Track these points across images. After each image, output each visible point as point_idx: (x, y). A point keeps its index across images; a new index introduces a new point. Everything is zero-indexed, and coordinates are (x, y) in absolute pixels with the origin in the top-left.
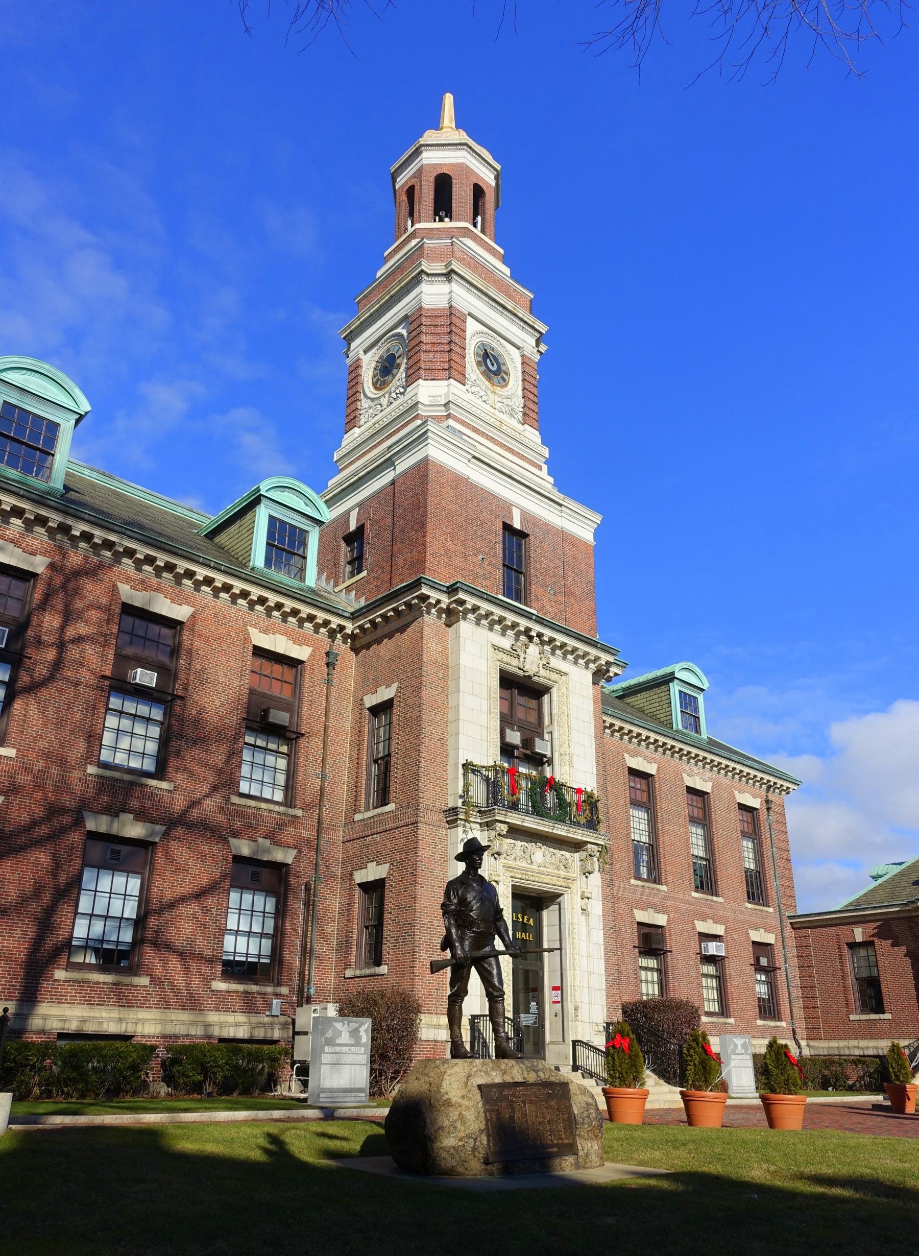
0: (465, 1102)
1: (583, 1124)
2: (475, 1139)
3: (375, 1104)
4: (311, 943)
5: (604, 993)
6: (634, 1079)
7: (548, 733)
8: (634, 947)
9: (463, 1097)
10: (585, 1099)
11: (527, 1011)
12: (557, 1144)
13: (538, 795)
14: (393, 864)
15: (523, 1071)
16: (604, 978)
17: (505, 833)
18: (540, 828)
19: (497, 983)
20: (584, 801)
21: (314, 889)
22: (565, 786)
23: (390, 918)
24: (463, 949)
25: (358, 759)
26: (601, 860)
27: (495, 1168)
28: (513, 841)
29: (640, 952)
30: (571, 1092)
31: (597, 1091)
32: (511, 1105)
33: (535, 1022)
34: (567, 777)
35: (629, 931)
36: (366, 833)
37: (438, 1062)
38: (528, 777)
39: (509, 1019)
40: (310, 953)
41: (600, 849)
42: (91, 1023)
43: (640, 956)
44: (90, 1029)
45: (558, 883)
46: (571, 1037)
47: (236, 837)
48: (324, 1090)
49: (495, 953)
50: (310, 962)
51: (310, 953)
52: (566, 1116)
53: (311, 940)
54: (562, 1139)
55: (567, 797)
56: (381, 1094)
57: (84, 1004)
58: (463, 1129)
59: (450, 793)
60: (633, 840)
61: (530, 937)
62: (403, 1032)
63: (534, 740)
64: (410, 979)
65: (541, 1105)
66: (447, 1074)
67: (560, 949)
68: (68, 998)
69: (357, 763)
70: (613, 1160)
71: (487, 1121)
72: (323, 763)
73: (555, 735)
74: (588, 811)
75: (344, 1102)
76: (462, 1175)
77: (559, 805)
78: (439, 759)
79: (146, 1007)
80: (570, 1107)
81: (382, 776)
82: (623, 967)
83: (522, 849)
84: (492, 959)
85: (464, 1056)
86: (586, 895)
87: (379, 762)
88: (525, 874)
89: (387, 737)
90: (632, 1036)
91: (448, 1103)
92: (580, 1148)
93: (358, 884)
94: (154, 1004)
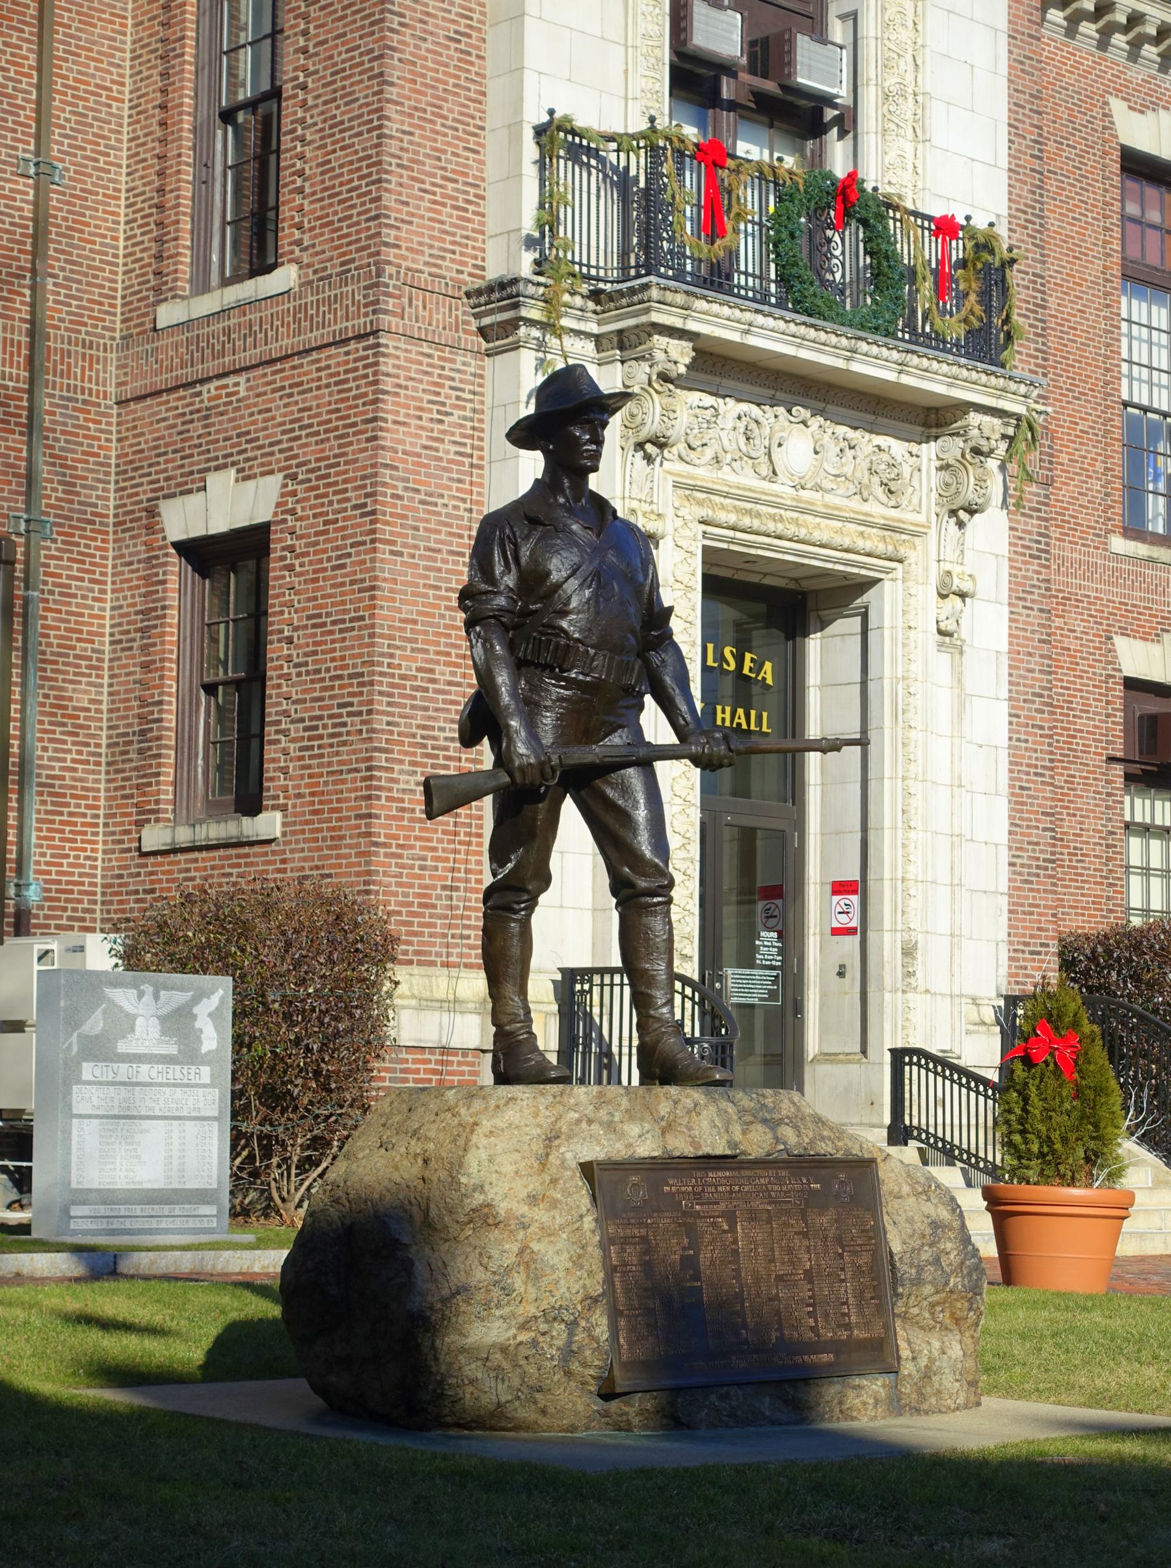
0: (540, 1215)
1: (918, 1282)
2: (572, 1325)
3: (249, 1238)
4: (22, 738)
5: (1003, 902)
6: (1087, 1159)
7: (842, 17)
8: (1111, 759)
9: (533, 1200)
10: (928, 1208)
11: (747, 959)
12: (831, 1340)
13: (803, 241)
14: (294, 477)
15: (728, 1123)
16: (1004, 856)
17: (682, 369)
18: (804, 354)
19: (647, 851)
20: (963, 264)
21: (27, 563)
22: (896, 208)
23: (289, 659)
24: (533, 736)
25: (163, 107)
26: (1012, 467)
27: (633, 1409)
28: (709, 400)
29: (1129, 778)
30: (884, 1189)
31: (973, 1201)
32: (688, 1225)
33: (772, 995)
34: (906, 177)
35: (1096, 706)
36: (200, 370)
37: (450, 1094)
38: (766, 176)
39: (686, 981)
40: (21, 773)
41: (1010, 431)
43: (1124, 289)
45: (861, 544)
46: (888, 1038)
48: (83, 1197)
49: (642, 752)
50: (20, 801)
51: (21, 773)
52: (864, 1259)
53: (23, 729)
54: (848, 1327)
55: (904, 250)
56: (269, 1210)
58: (532, 1293)
59: (490, 229)
60: (1126, 404)
61: (761, 721)
62: (336, 1019)
63: (792, 42)
64: (358, 854)
65: (786, 1224)
66: (479, 1130)
67: (863, 742)
69: (163, 124)
70: (1008, 1391)
71: (610, 1271)
72: (38, 121)
73: (870, 26)
74: (973, 297)
75: (150, 1232)
76: (528, 1428)
77: (876, 276)
78: (451, 109)
80: (876, 1234)
81: (251, 171)
82: (1068, 826)
83: (741, 426)
84: (631, 771)
85: (539, 1076)
86: (957, 584)
87: (241, 117)
88: (749, 512)
89: (267, 29)
90: (1087, 1027)
91: (485, 1217)
92: (905, 1353)
93: (175, 545)
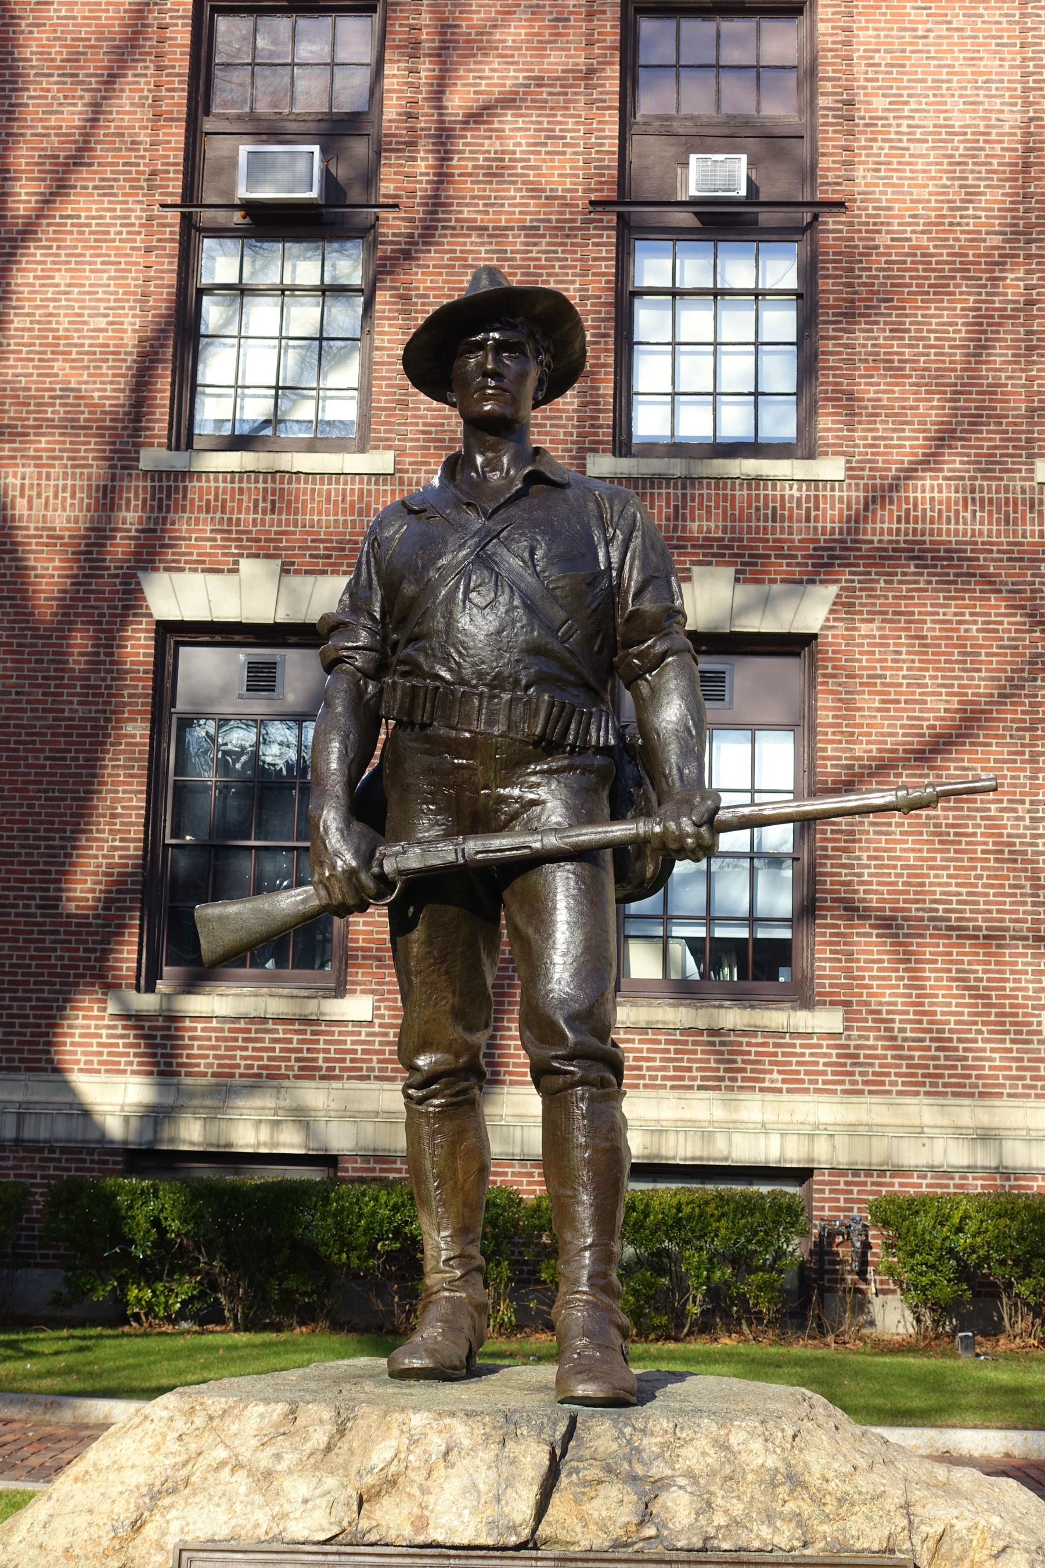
42: (681, 1135)
44: (681, 1153)
57: (664, 1087)
79: (645, 1086)
94: (866, 1083)
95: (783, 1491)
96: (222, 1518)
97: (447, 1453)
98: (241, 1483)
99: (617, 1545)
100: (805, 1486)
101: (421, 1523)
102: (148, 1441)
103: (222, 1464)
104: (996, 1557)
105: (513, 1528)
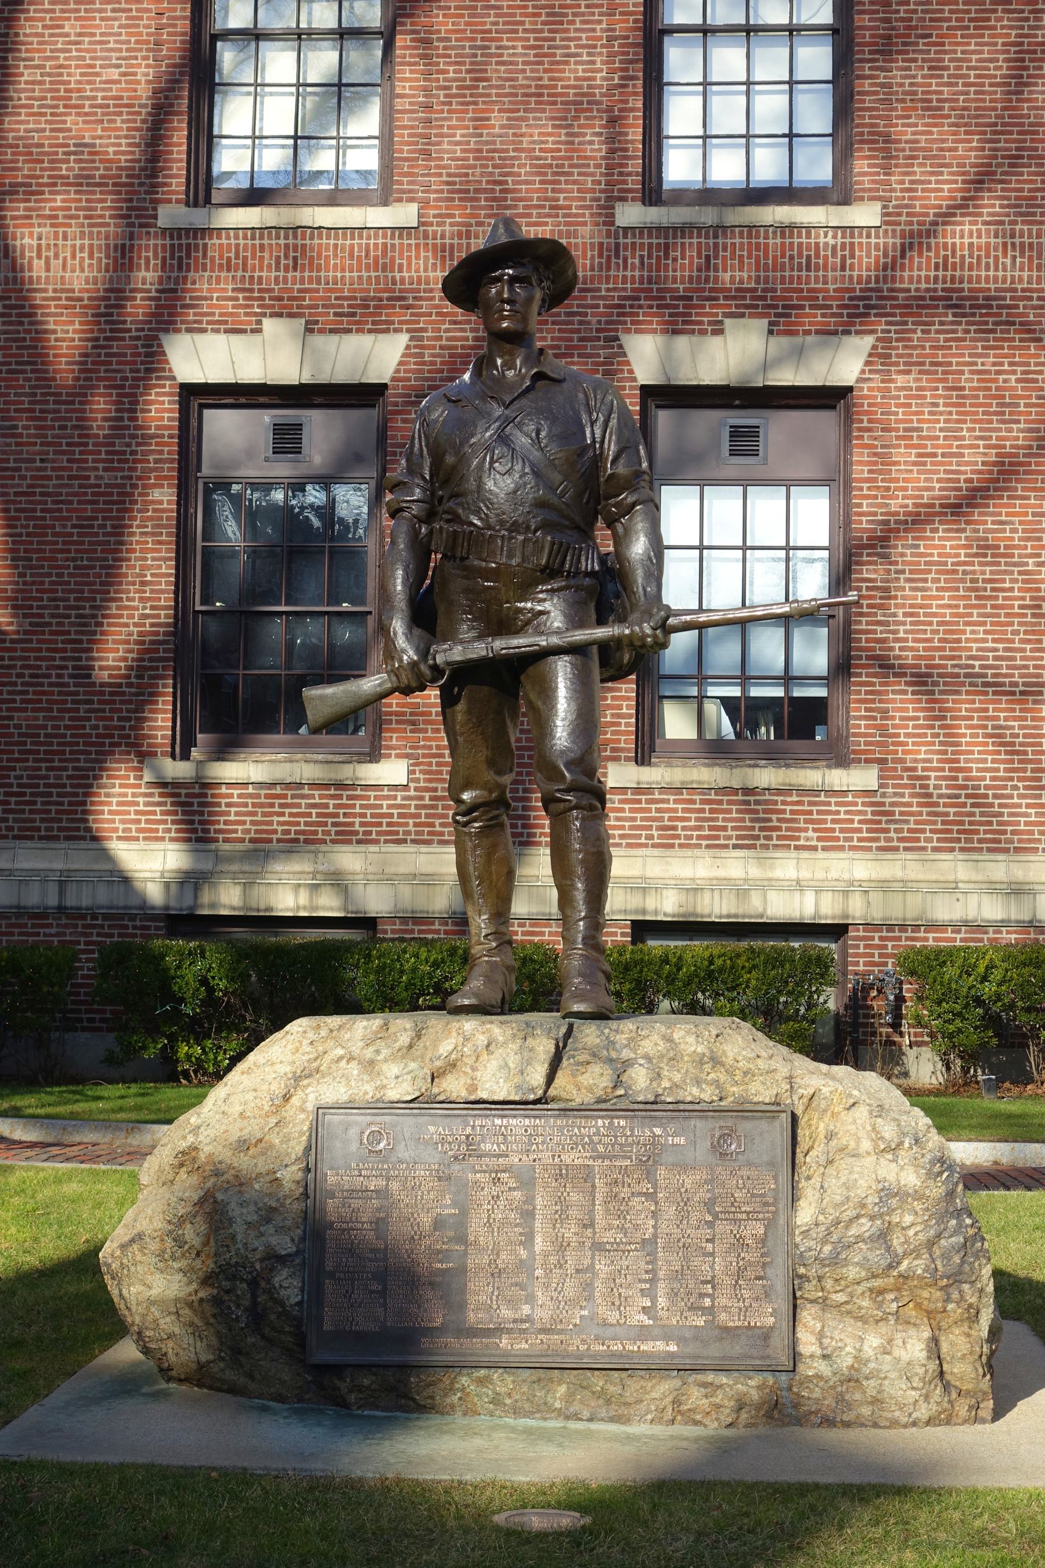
42: (716, 894)
47: (387, 331)
57: (699, 846)
68: (655, 833)
79: (681, 846)
94: (901, 840)
95: (707, 1067)
96: (343, 1090)
97: (488, 1046)
98: (354, 1069)
99: (599, 1101)
100: (722, 1064)
101: (473, 1088)
102: (290, 1047)
103: (341, 1058)
104: (848, 1109)
105: (532, 1090)
